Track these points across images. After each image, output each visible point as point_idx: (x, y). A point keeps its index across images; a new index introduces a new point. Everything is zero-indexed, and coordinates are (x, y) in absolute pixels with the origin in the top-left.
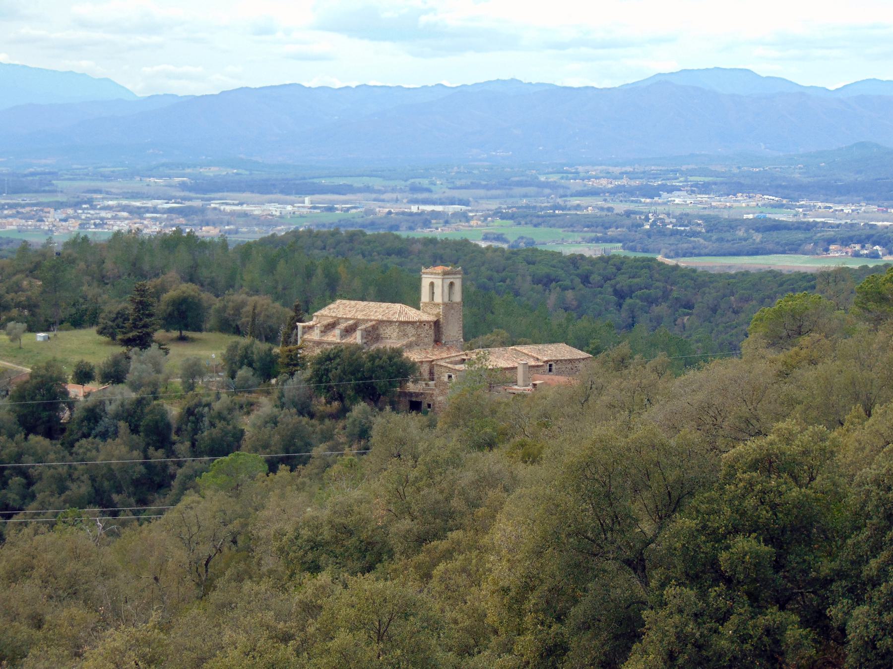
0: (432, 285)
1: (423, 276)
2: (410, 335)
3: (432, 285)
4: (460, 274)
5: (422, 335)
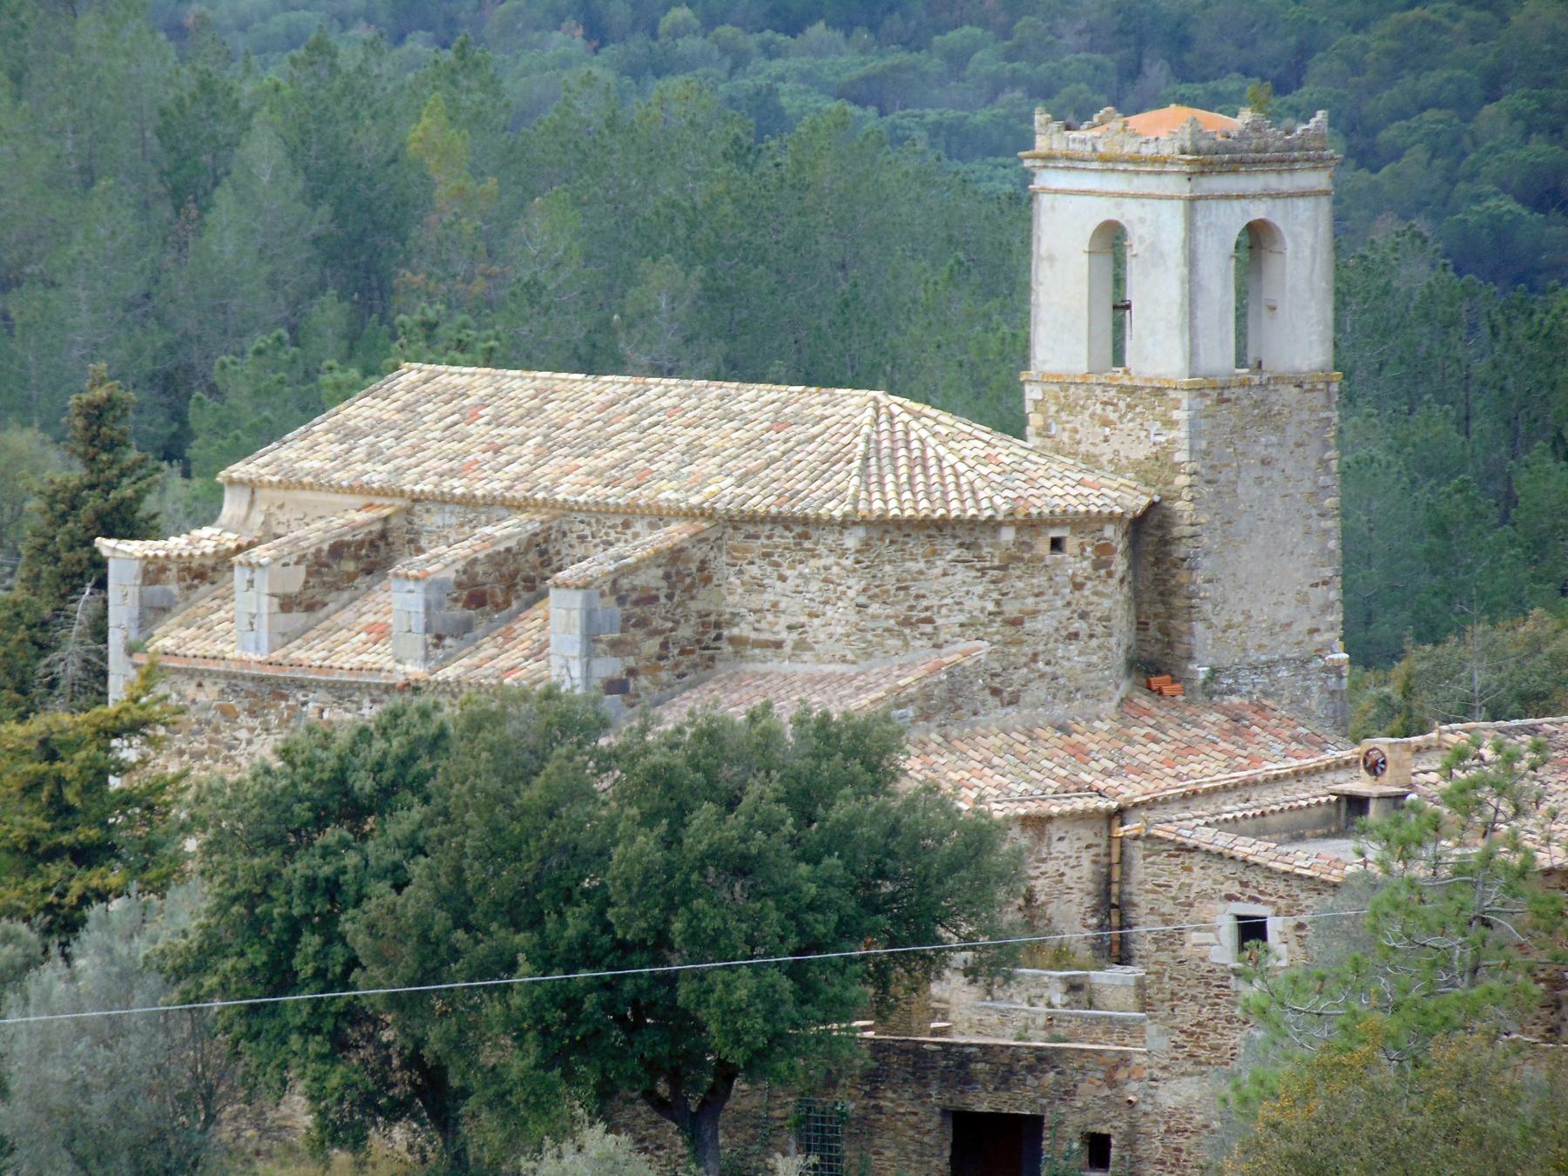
0: (1111, 239)
1: (1047, 179)
2: (948, 622)
3: (1111, 239)
4: (1317, 162)
5: (1043, 624)
